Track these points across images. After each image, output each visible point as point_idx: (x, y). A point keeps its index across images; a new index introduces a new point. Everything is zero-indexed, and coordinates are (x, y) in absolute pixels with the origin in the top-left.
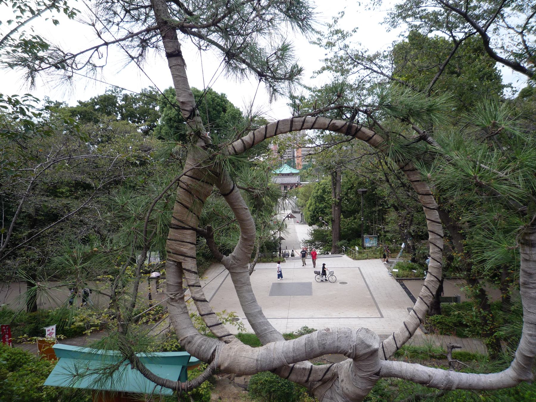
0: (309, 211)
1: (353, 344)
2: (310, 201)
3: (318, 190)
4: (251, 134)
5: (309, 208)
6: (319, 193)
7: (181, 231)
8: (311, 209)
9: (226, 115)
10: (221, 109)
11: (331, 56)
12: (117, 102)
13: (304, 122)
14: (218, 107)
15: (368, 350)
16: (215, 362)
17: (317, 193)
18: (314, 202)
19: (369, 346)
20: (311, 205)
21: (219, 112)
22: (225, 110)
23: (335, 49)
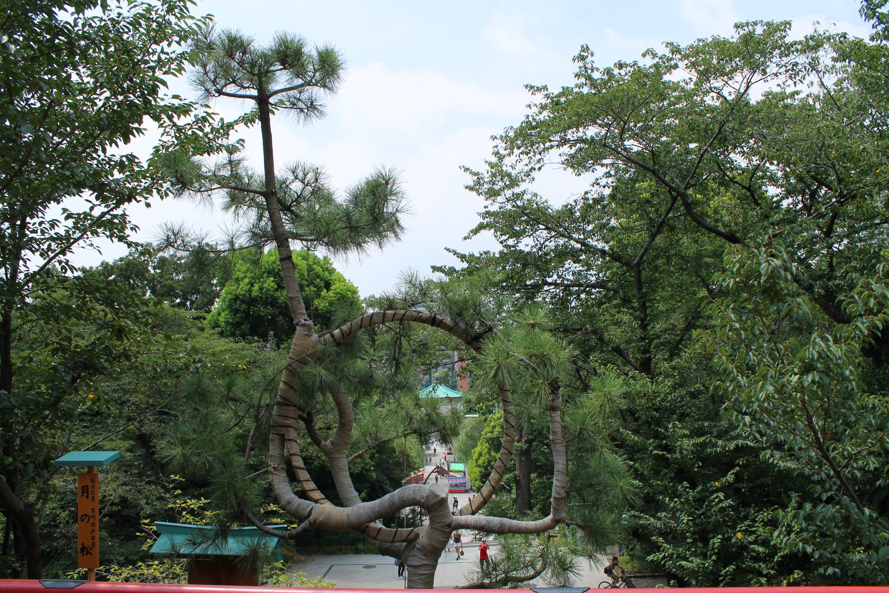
0: (479, 466)
1: (425, 495)
2: (478, 449)
3: (494, 427)
4: (349, 324)
5: (477, 460)
6: (495, 434)
7: (285, 407)
8: (480, 462)
9: (331, 293)
10: (322, 284)
11: (494, 208)
12: (148, 271)
13: (394, 315)
14: (318, 280)
15: (437, 500)
16: (312, 517)
17: (492, 432)
18: (486, 450)
19: (437, 496)
20: (480, 455)
21: (319, 289)
22: (328, 286)
23: (500, 199)
